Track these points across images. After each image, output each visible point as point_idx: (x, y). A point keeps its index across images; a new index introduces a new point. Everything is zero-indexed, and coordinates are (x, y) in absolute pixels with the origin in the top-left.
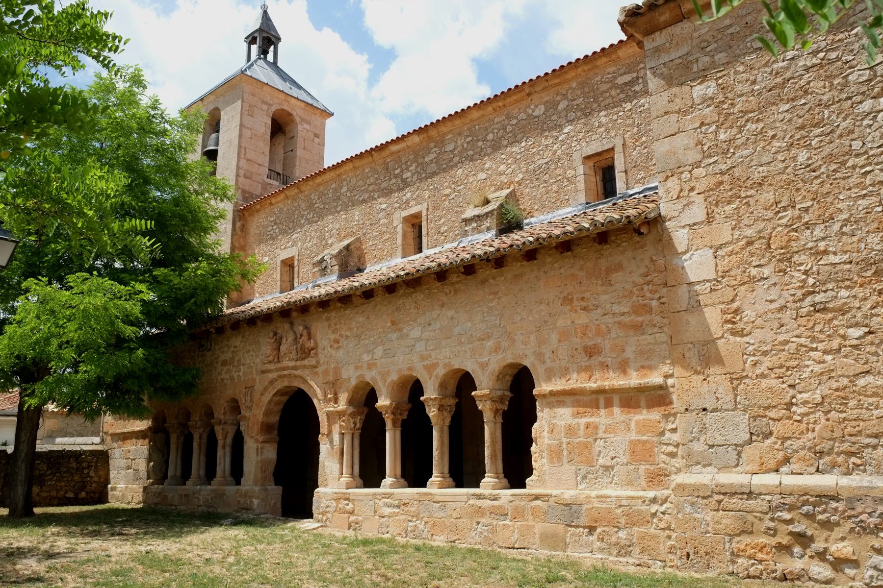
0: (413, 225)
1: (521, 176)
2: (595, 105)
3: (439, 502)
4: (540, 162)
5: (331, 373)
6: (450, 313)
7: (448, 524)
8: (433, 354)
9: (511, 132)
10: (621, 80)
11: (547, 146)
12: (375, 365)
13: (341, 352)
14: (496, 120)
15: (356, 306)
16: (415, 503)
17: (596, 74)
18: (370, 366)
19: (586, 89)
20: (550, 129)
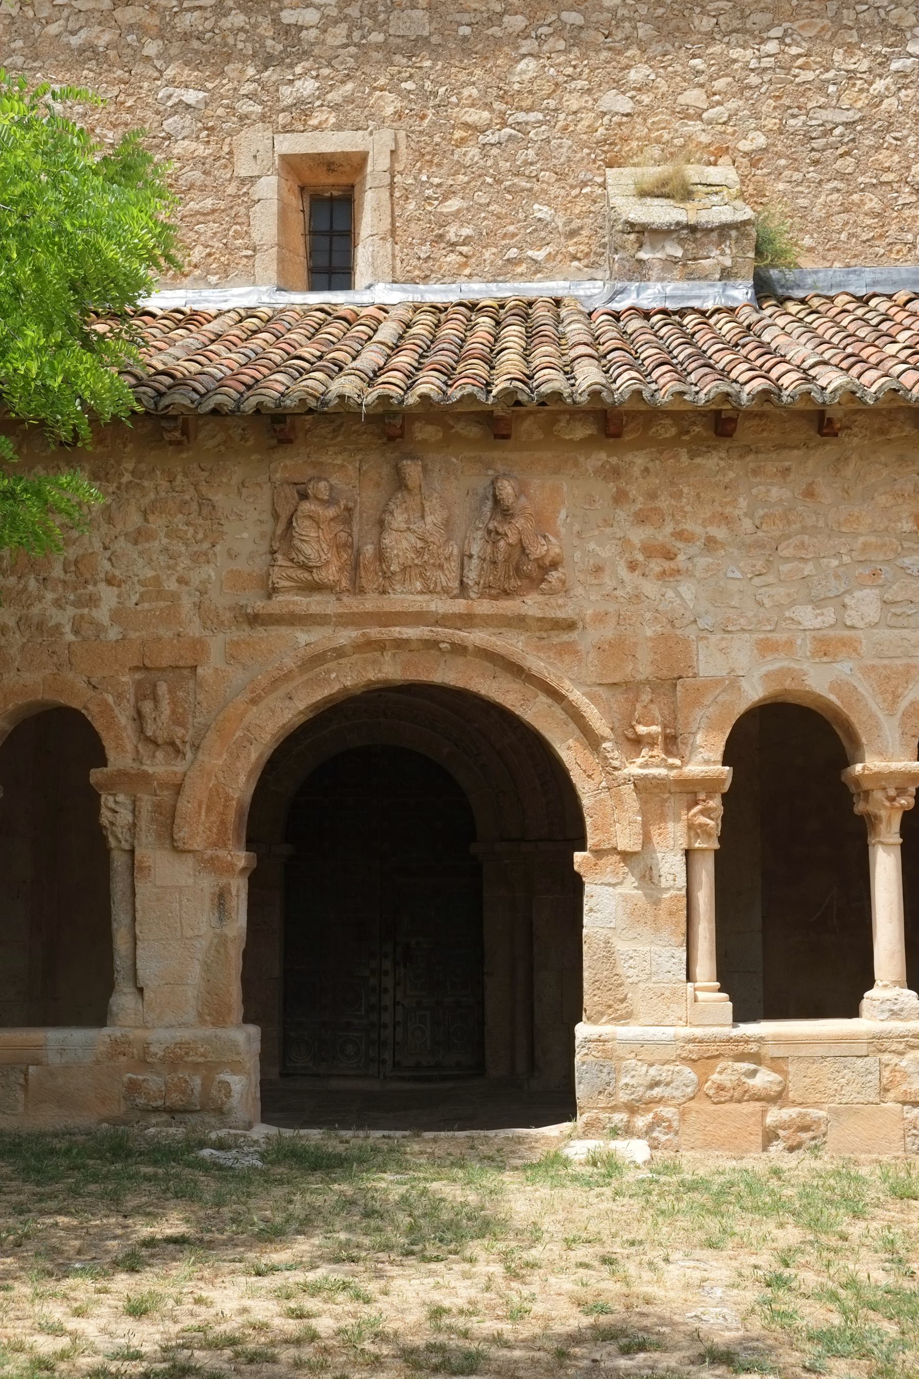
0: (302, 189)
1: (761, 140)
11: (852, 75)
13: (687, 590)
15: (748, 450)
18: (826, 648)
20: (865, 32)
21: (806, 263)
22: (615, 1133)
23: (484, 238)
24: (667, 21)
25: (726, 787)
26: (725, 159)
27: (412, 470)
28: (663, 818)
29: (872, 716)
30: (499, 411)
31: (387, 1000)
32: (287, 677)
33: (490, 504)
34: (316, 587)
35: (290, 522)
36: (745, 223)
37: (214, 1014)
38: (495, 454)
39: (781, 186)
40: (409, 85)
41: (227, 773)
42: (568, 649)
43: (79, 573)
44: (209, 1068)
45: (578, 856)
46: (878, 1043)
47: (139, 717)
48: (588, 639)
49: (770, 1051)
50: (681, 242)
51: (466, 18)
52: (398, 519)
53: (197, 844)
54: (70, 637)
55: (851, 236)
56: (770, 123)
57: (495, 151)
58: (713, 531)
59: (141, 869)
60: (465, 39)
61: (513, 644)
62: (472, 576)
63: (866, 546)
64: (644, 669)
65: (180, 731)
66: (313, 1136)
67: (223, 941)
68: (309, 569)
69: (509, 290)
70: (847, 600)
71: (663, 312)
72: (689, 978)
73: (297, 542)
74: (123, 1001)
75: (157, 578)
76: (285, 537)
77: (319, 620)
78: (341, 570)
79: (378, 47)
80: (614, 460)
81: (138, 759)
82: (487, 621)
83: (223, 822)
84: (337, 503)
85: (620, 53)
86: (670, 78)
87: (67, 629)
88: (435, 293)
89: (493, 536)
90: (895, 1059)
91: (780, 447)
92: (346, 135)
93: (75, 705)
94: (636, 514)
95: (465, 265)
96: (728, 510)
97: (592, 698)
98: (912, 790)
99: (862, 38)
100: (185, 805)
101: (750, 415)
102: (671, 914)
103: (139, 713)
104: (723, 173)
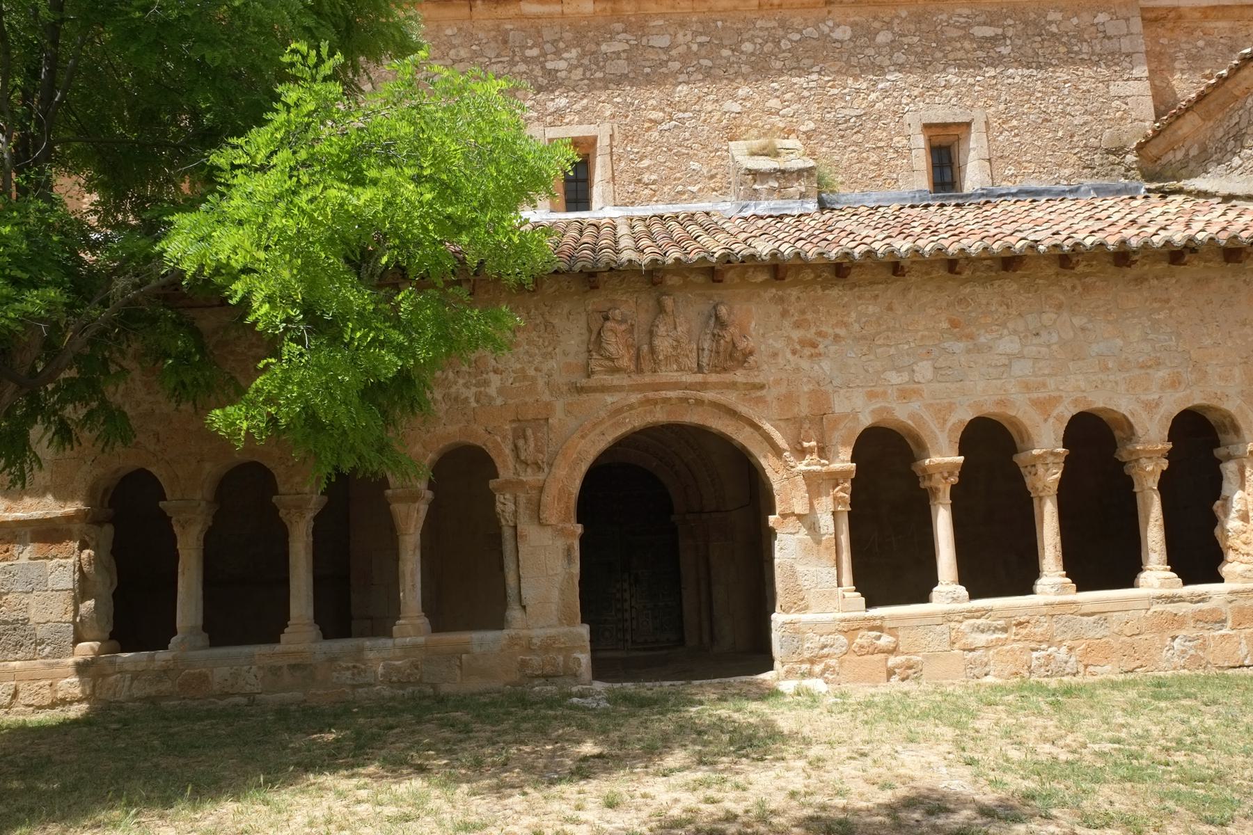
1: (812, 125)
2: (939, 55)
3: (1093, 614)
4: (847, 112)
5: (804, 402)
6: (1078, 321)
7: (1116, 645)
8: (1051, 383)
9: (789, 51)
10: (980, 31)
11: (858, 91)
12: (917, 392)
13: (826, 365)
14: (759, 24)
15: (854, 285)
16: (1043, 619)
17: (942, 11)
18: (905, 394)
19: (924, 26)
21: (841, 190)
22: (803, 675)
23: (665, 180)
24: (757, 64)
25: (853, 476)
26: (793, 135)
27: (668, 302)
28: (819, 495)
29: (932, 432)
30: (718, 267)
31: (627, 605)
32: (602, 422)
33: (712, 322)
34: (616, 370)
35: (599, 333)
36: (811, 168)
37: (566, 619)
38: (714, 292)
39: (824, 149)
40: (618, 100)
41: (567, 479)
42: (760, 400)
43: (477, 367)
44: (568, 650)
45: (772, 518)
46: (947, 616)
47: (516, 448)
48: (771, 394)
49: (887, 624)
50: (777, 179)
51: (648, 64)
52: (662, 330)
53: (553, 521)
54: (474, 404)
55: (864, 175)
56: (816, 116)
57: (667, 134)
58: (838, 331)
59: (522, 537)
60: (648, 74)
61: (730, 398)
62: (705, 361)
63: (923, 337)
64: (804, 409)
65: (541, 456)
66: (630, 687)
67: (571, 576)
68: (612, 360)
69: (680, 208)
70: (915, 367)
71: (771, 216)
72: (839, 585)
73: (604, 345)
74: (514, 613)
75: (523, 369)
76: (596, 343)
77: (619, 389)
78: (630, 360)
79: (600, 80)
80: (780, 293)
81: (517, 473)
82: (715, 386)
83: (567, 507)
84: (626, 322)
85: (733, 81)
86: (760, 94)
87: (472, 400)
88: (638, 211)
89: (716, 337)
90: (958, 625)
91: (872, 283)
92: (585, 126)
93: (479, 443)
94: (795, 323)
95: (654, 195)
96: (845, 319)
97: (777, 427)
98: (957, 473)
99: (862, 72)
100: (546, 499)
101: (860, 266)
102: (827, 548)
103: (516, 446)
104: (792, 142)
